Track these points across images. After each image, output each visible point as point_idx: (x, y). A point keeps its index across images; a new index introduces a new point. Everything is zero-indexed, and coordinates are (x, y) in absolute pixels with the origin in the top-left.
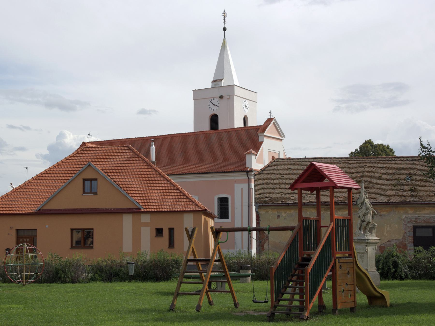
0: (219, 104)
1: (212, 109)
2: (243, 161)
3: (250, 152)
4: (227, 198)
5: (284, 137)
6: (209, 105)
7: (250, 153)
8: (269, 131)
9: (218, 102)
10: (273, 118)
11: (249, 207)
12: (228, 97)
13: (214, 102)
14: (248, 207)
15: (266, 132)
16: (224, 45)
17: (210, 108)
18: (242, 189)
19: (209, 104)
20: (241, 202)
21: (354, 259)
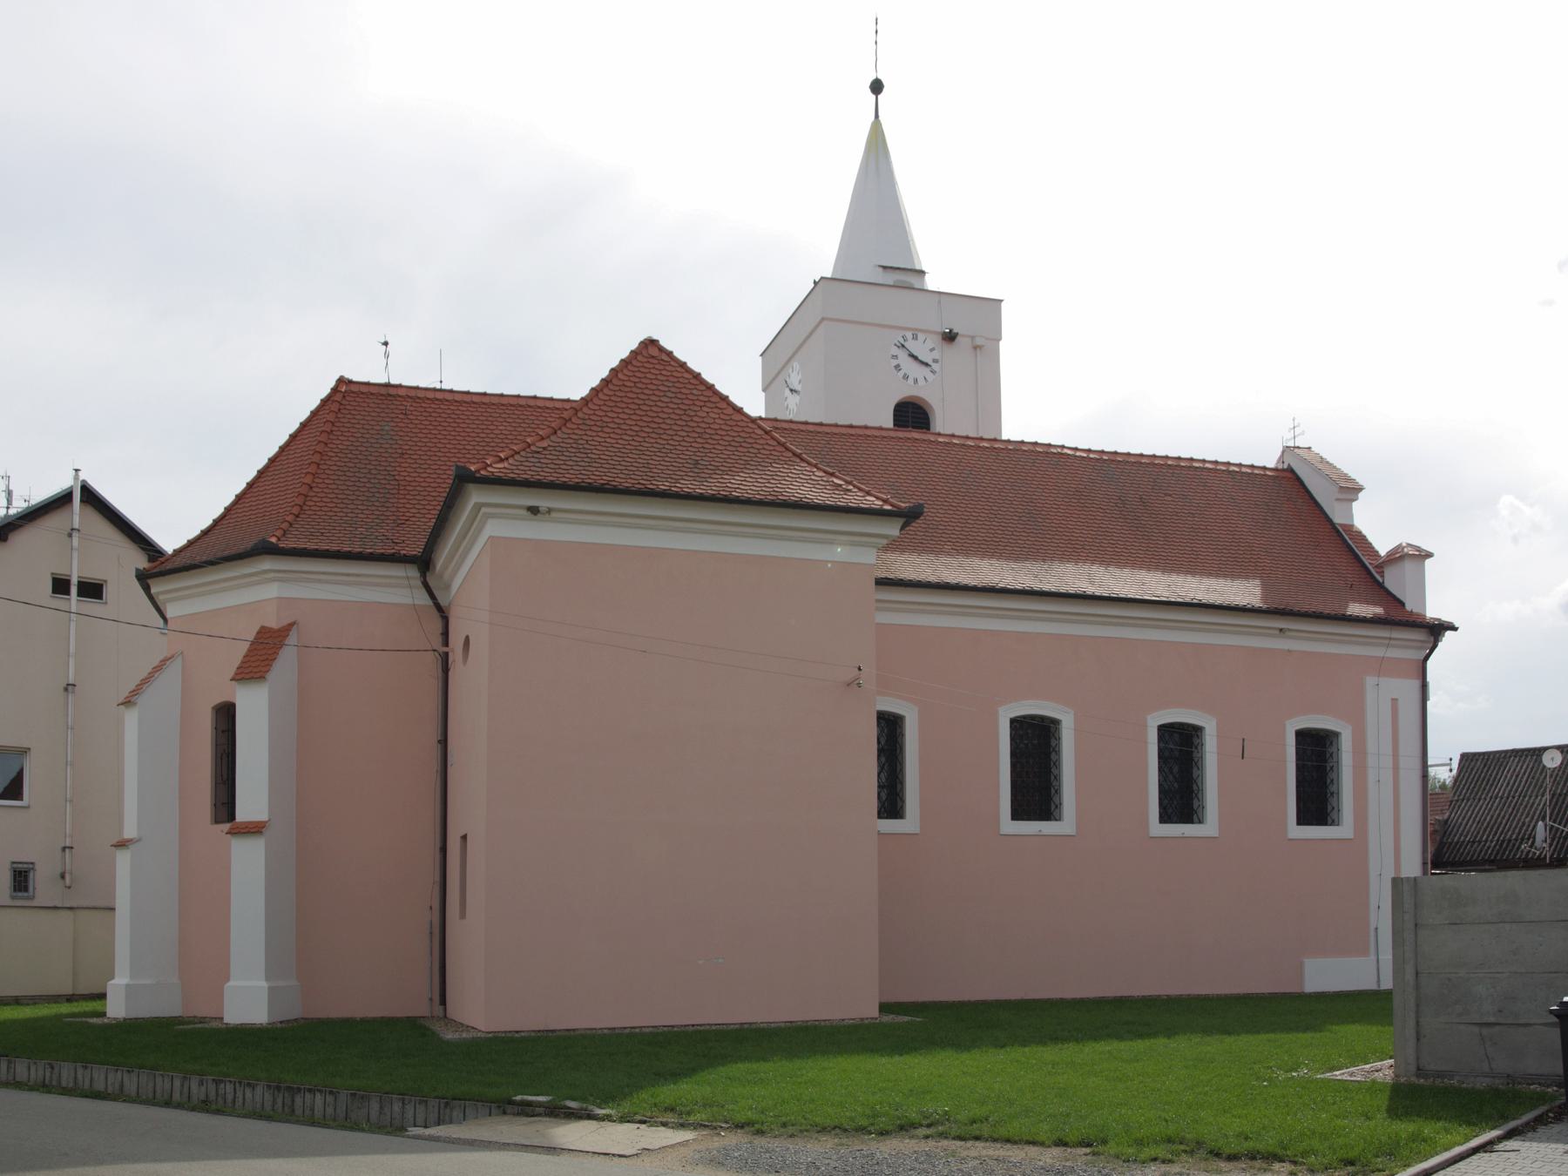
1: (906, 377)
6: (895, 357)
9: (935, 354)
13: (912, 346)
14: (438, 856)
16: (877, 143)
17: (897, 367)
19: (895, 351)
21: (1044, 1131)
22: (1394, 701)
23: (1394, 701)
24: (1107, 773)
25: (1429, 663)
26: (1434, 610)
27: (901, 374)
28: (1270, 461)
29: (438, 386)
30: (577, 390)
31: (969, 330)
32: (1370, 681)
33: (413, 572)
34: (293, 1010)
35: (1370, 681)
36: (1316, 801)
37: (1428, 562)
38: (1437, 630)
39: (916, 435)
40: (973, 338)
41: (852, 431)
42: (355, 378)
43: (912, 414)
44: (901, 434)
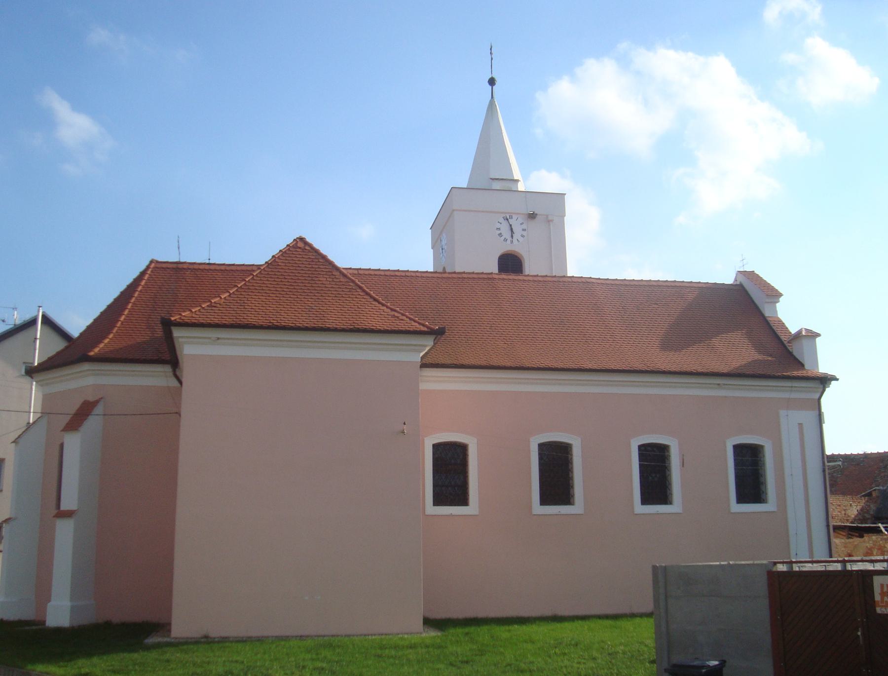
16: (492, 106)
22: (800, 425)
23: (800, 425)
24: (606, 475)
25: (823, 400)
26: (824, 368)
27: (502, 238)
28: (728, 278)
29: (207, 262)
30: (342, 262)
31: (545, 213)
32: (782, 413)
33: (168, 369)
34: (86, 619)
35: (782, 413)
36: (751, 487)
37: (818, 339)
38: (825, 381)
39: (512, 277)
40: (547, 216)
41: (454, 275)
42: (160, 260)
43: (510, 263)
44: (504, 276)
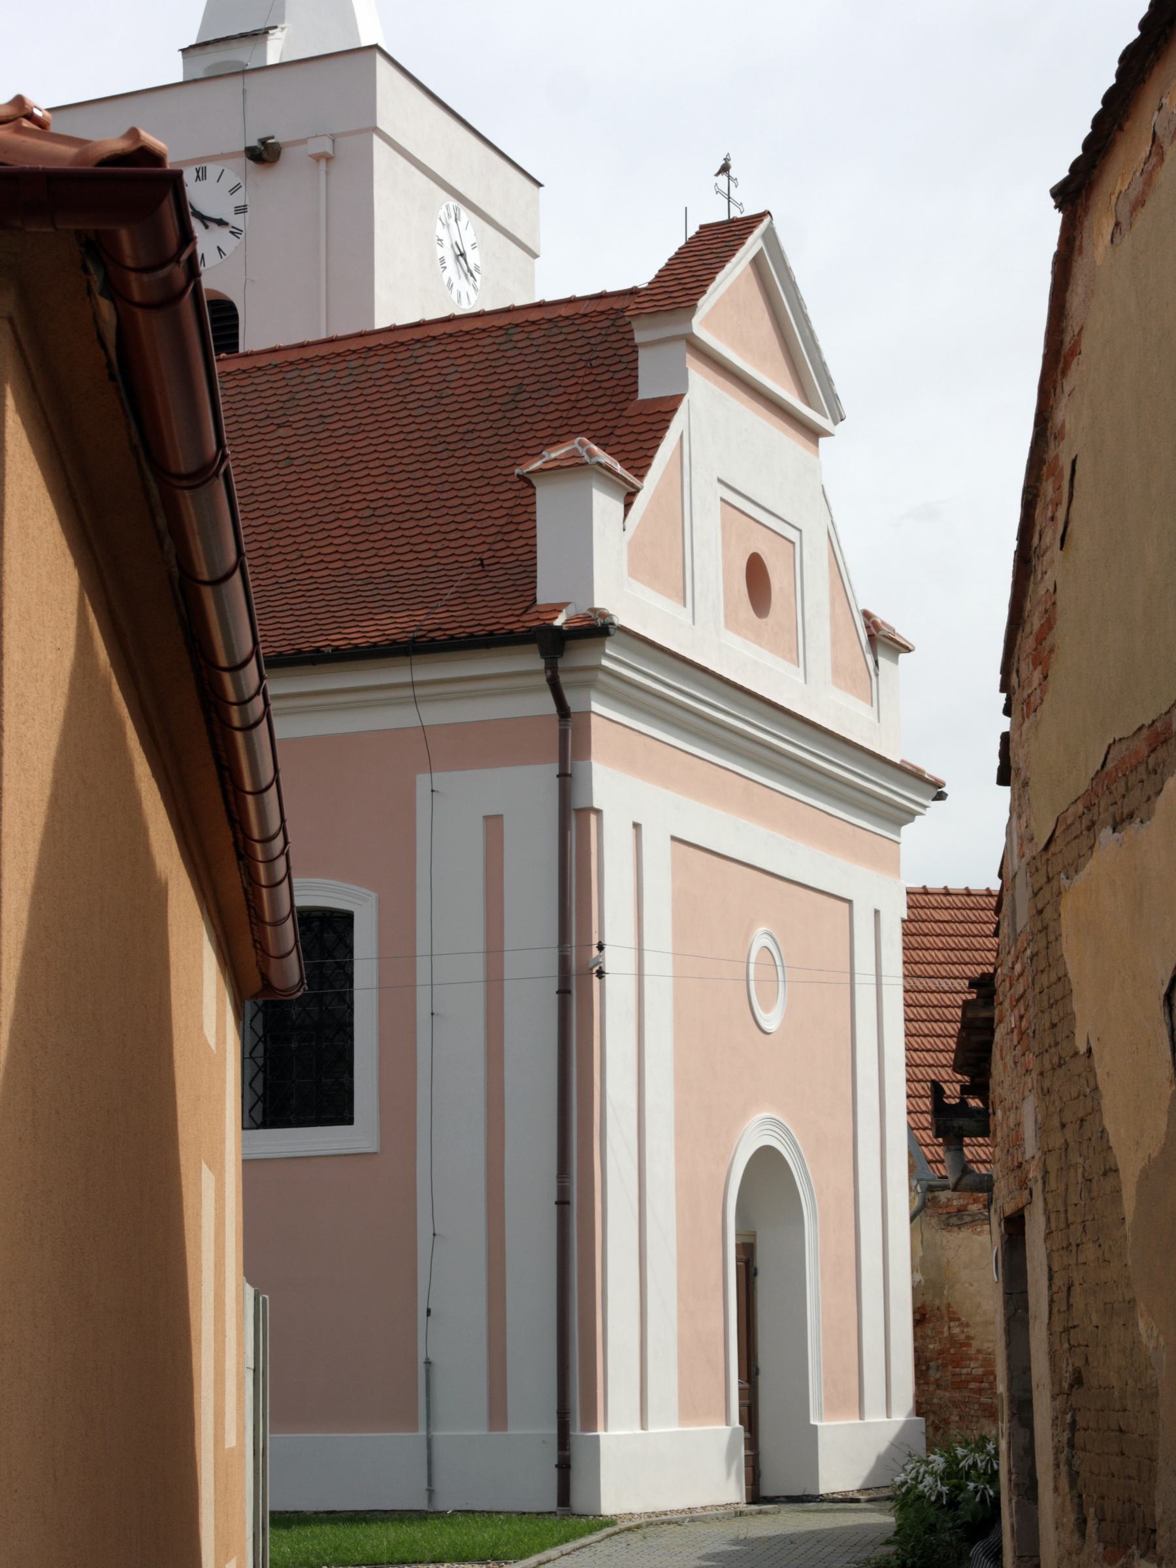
0: (241, 210)
2: (511, 551)
3: (574, 455)
4: (347, 918)
5: (838, 417)
7: (576, 466)
8: (724, 311)
9: (239, 199)
10: (749, 223)
11: (564, 992)
12: (326, 146)
14: (554, 999)
15: (706, 304)
18: (493, 824)
20: (478, 941)
